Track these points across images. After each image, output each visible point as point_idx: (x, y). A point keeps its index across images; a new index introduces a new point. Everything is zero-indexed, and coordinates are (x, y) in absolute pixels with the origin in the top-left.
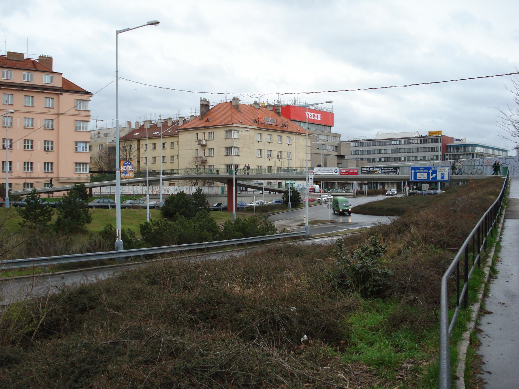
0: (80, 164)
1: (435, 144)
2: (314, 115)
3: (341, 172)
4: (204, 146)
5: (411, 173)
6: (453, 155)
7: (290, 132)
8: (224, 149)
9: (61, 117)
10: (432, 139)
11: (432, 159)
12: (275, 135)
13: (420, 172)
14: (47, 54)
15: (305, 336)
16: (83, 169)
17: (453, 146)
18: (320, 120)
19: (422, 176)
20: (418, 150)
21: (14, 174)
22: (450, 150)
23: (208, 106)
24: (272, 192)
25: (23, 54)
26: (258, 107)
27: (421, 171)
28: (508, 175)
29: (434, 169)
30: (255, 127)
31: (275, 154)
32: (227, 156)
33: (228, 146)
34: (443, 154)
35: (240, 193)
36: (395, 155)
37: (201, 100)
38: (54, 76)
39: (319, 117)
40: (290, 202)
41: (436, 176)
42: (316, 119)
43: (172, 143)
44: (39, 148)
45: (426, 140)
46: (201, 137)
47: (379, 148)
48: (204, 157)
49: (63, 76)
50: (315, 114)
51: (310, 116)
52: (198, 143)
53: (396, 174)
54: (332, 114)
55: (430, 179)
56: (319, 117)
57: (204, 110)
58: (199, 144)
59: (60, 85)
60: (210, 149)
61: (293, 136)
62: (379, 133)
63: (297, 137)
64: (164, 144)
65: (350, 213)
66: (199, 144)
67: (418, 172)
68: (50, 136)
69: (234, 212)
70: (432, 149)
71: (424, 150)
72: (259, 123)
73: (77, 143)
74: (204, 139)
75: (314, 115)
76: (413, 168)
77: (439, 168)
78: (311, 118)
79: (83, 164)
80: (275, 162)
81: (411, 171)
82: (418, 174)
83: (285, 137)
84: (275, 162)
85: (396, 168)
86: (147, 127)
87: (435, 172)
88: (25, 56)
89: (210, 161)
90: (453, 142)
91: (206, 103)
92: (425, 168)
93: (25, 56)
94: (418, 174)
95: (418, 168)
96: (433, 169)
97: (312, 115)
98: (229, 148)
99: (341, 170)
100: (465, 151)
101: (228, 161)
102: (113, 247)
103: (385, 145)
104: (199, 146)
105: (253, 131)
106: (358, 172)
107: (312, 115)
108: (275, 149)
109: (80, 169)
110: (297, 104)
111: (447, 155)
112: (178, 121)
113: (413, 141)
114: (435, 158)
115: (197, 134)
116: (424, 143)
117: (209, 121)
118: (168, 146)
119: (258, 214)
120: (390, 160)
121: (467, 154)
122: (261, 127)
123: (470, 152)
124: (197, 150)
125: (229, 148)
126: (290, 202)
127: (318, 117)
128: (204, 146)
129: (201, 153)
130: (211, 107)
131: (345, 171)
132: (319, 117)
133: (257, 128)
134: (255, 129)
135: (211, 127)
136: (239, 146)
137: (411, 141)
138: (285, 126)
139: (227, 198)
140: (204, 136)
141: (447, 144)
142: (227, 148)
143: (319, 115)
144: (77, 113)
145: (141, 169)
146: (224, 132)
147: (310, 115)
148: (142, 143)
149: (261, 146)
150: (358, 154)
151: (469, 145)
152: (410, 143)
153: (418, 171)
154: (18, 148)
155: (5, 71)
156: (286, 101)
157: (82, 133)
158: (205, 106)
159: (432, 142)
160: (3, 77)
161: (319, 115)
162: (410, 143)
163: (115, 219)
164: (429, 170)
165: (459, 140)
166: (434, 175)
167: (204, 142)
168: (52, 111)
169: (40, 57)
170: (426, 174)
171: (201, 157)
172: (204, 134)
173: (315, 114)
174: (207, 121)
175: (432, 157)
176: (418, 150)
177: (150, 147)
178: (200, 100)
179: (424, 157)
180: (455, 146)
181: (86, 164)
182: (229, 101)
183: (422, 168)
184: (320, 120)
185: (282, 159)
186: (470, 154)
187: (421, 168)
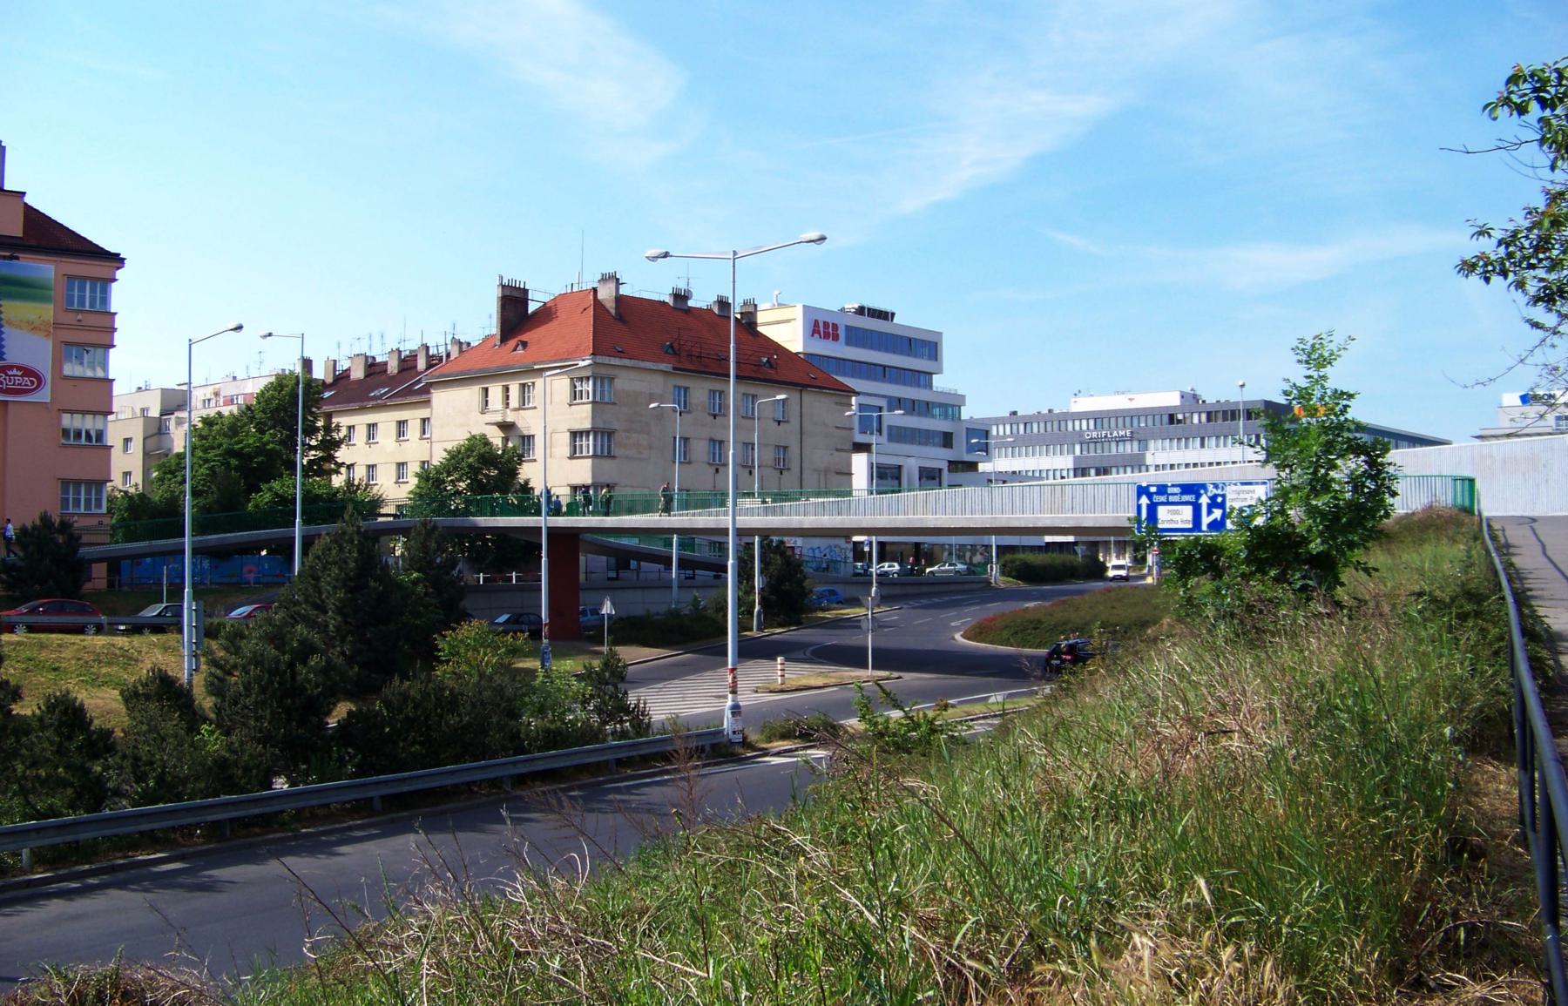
0: (77, 483)
5: (1139, 507)
13: (1168, 503)
16: (88, 501)
19: (1174, 517)
27: (1171, 499)
28: (190, 412)
29: (1215, 491)
32: (571, 458)
35: (617, 578)
49: (28, 200)
55: (1204, 527)
59: (18, 231)
63: (808, 398)
64: (401, 424)
67: (1163, 504)
72: (684, 354)
76: (1142, 491)
77: (1234, 488)
81: (1139, 497)
82: (1162, 512)
91: (516, 294)
92: (1187, 489)
95: (1162, 489)
96: (1212, 491)
109: (77, 502)
115: (486, 390)
118: (413, 430)
122: (689, 366)
130: (532, 307)
133: (674, 369)
134: (666, 372)
153: (1162, 499)
182: (590, 286)
183: (1177, 490)
187: (1170, 490)
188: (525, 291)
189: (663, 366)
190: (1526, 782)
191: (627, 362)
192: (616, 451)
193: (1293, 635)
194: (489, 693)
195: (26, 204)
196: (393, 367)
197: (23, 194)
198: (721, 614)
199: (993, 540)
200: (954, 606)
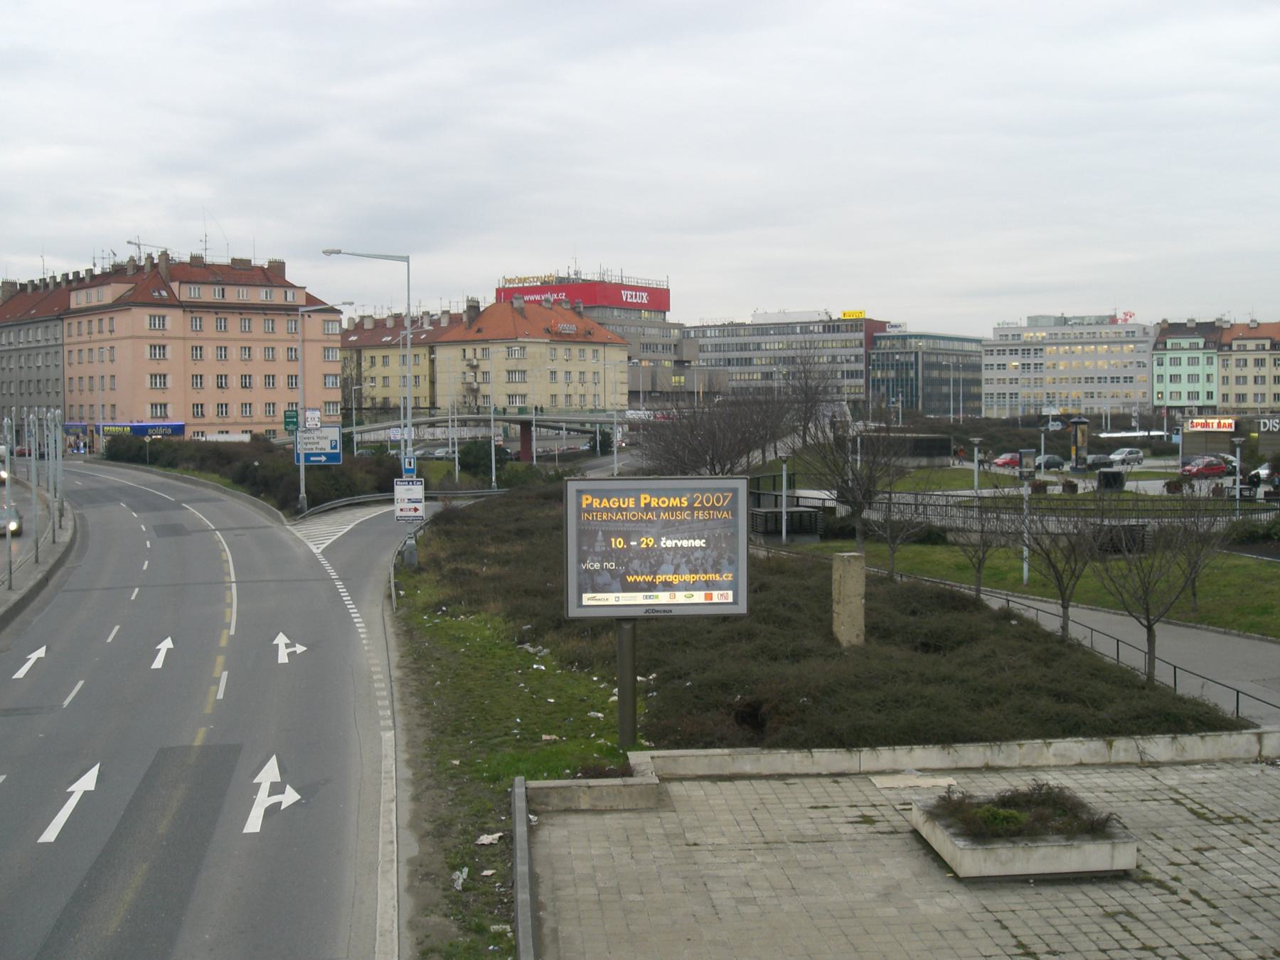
0: (329, 403)
1: (852, 334)
4: (474, 368)
6: (883, 354)
8: (505, 374)
9: (306, 344)
12: (575, 349)
17: (884, 338)
21: (255, 419)
23: (478, 308)
24: (572, 433)
26: (550, 306)
31: (575, 377)
32: (508, 382)
33: (510, 369)
34: (866, 352)
37: (468, 301)
38: (296, 291)
40: (598, 448)
43: (415, 355)
44: (282, 385)
45: (838, 326)
46: (469, 354)
47: (757, 339)
48: (475, 384)
49: (307, 290)
51: (629, 296)
52: (465, 363)
54: (667, 291)
58: (467, 365)
61: (601, 349)
62: (758, 312)
63: (607, 349)
65: (1142, 459)
66: (467, 365)
68: (294, 369)
69: (535, 462)
73: (325, 376)
79: (333, 403)
80: (576, 388)
83: (589, 350)
84: (576, 388)
86: (368, 325)
88: (253, 263)
89: (485, 389)
91: (476, 304)
100: (905, 348)
101: (512, 389)
102: (490, 486)
103: (767, 335)
105: (544, 346)
107: (632, 296)
108: (575, 368)
109: (329, 410)
110: (607, 279)
111: (874, 354)
112: (422, 317)
113: (816, 328)
114: (853, 358)
115: (464, 350)
116: (834, 332)
119: (561, 464)
120: (844, 328)
121: (907, 353)
122: (556, 339)
123: (913, 349)
124: (464, 373)
126: (598, 448)
127: (644, 298)
128: (474, 368)
129: (470, 378)
130: (481, 309)
135: (486, 341)
136: (524, 369)
137: (811, 328)
138: (590, 333)
139: (519, 443)
140: (475, 354)
143: (645, 295)
144: (325, 337)
146: (505, 349)
147: (626, 295)
148: (367, 354)
150: (720, 351)
151: (911, 336)
152: (812, 332)
156: (590, 273)
157: (332, 364)
159: (847, 331)
161: (645, 295)
162: (812, 332)
163: (459, 472)
165: (896, 326)
167: (475, 363)
168: (296, 336)
171: (470, 383)
172: (475, 350)
174: (479, 331)
175: (848, 358)
177: (379, 361)
181: (337, 403)
186: (912, 352)
188: (478, 302)
189: (546, 341)
190: (1146, 498)
191: (532, 340)
192: (527, 379)
193: (448, 904)
195: (307, 293)
196: (390, 324)
197: (305, 288)
198: (1135, 728)
199: (720, 476)
200: (1067, 884)
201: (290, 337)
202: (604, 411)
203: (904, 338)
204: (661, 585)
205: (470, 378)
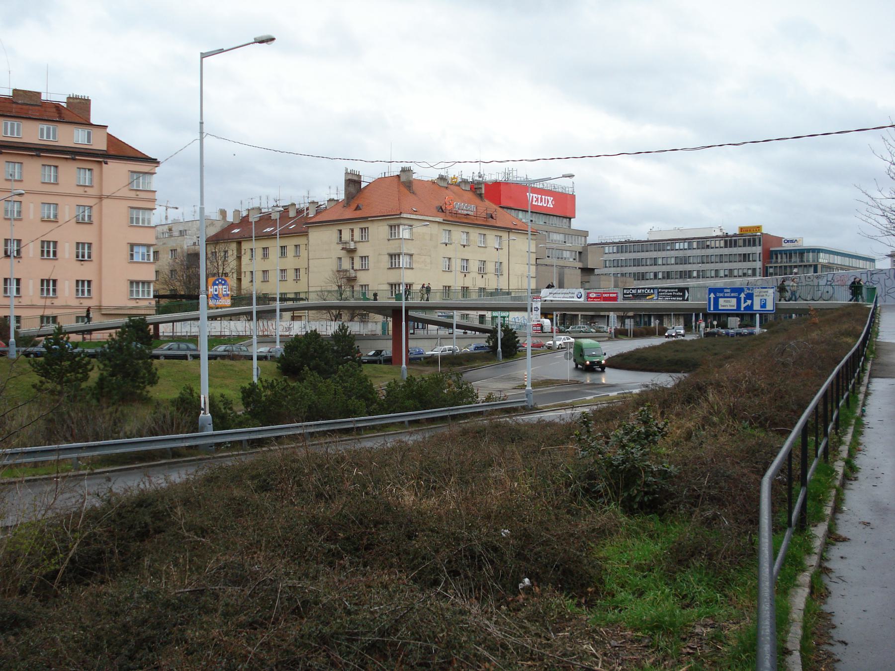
0: (138, 283)
1: (749, 248)
2: (541, 198)
3: (588, 297)
4: (351, 252)
5: (710, 299)
6: (781, 267)
7: (501, 228)
8: (387, 258)
9: (105, 202)
10: (744, 240)
11: (745, 275)
12: (475, 233)
13: (724, 297)
14: (81, 93)
15: (527, 580)
16: (143, 291)
18: (552, 206)
20: (721, 258)
22: (777, 258)
23: (359, 183)
24: (469, 332)
25: (39, 94)
26: (445, 185)
27: (726, 295)
28: (876, 302)
30: (440, 220)
31: (474, 266)
32: (391, 268)
33: (393, 251)
34: (763, 265)
35: (414, 333)
36: (681, 268)
37: (347, 173)
38: (94, 131)
39: (550, 201)
40: (499, 349)
41: (752, 304)
42: (545, 205)
43: (296, 246)
44: (67, 256)
45: (735, 241)
46: (346, 236)
47: (654, 254)
48: (352, 271)
49: (109, 131)
50: (543, 197)
51: (535, 199)
52: (341, 246)
53: (683, 300)
54: (573, 197)
55: (742, 309)
56: (550, 201)
57: (352, 189)
58: (343, 249)
59: (103, 147)
60: (362, 257)
61: (505, 235)
62: (654, 230)
63: (512, 236)
64: (283, 248)
66: (343, 249)
67: (722, 297)
68: (86, 234)
69: (404, 365)
70: (745, 257)
71: (731, 258)
72: (447, 212)
73: (132, 246)
74: (352, 240)
75: (541, 198)
76: (712, 290)
77: (758, 290)
78: (536, 204)
79: (143, 283)
80: (474, 279)
81: (709, 294)
82: (721, 301)
83: (491, 236)
84: (474, 279)
85: (682, 290)
86: (253, 219)
87: (750, 297)
88: (44, 97)
89: (363, 278)
90: (781, 246)
91: (355, 178)
92: (733, 290)
93: (44, 97)
94: (720, 300)
95: (721, 290)
96: (747, 291)
97: (537, 199)
98: (395, 255)
99: (588, 293)
100: (802, 261)
101: (393, 277)
102: (195, 426)
103: (663, 250)
104: (344, 252)
105: (436, 226)
106: (617, 296)
107: (537, 199)
108: (475, 258)
109: (138, 292)
110: (512, 179)
111: (771, 267)
113: (713, 243)
114: (750, 272)
115: (340, 231)
116: (731, 247)
117: (360, 209)
118: (290, 251)
119: (445, 369)
121: (805, 266)
122: (451, 219)
123: (811, 262)
124: (340, 259)
125: (395, 255)
126: (499, 349)
127: (549, 203)
128: (351, 252)
129: (346, 265)
130: (363, 185)
131: (595, 295)
132: (550, 203)
133: (444, 220)
134: (439, 222)
135: (365, 219)
136: (412, 252)
137: (708, 243)
138: (492, 217)
139: (391, 342)
140: (352, 235)
141: (771, 249)
142: (391, 256)
143: (551, 199)
144: (133, 194)
145: (243, 292)
146: (387, 228)
147: (534, 199)
148: (245, 246)
149: (449, 252)
150: (618, 266)
151: (809, 250)
152: (708, 246)
153: (721, 295)
154: (31, 255)
155: (9, 123)
156: (493, 174)
157: (142, 230)
158: (353, 182)
159: (744, 245)
160: (6, 132)
161: (551, 199)
162: (708, 246)
163: (198, 378)
164: (740, 294)
165: (792, 241)
166: (749, 302)
167: (352, 246)
168: (90, 191)
169: (69, 98)
170: (734, 301)
171: (346, 271)
172: (352, 230)
173: (543, 197)
174: (358, 208)
175: (745, 271)
176: (721, 258)
177: (259, 253)
178: (344, 172)
179: (731, 271)
180: (785, 252)
181: (149, 283)
182: (396, 174)
183: (729, 291)
184: (552, 206)
185: (486, 274)
186: (811, 266)
187: (725, 291)
194: (523, 487)
201: (80, 191)
202: (509, 293)
203: (802, 252)
204: (402, 173)
205: (346, 265)
